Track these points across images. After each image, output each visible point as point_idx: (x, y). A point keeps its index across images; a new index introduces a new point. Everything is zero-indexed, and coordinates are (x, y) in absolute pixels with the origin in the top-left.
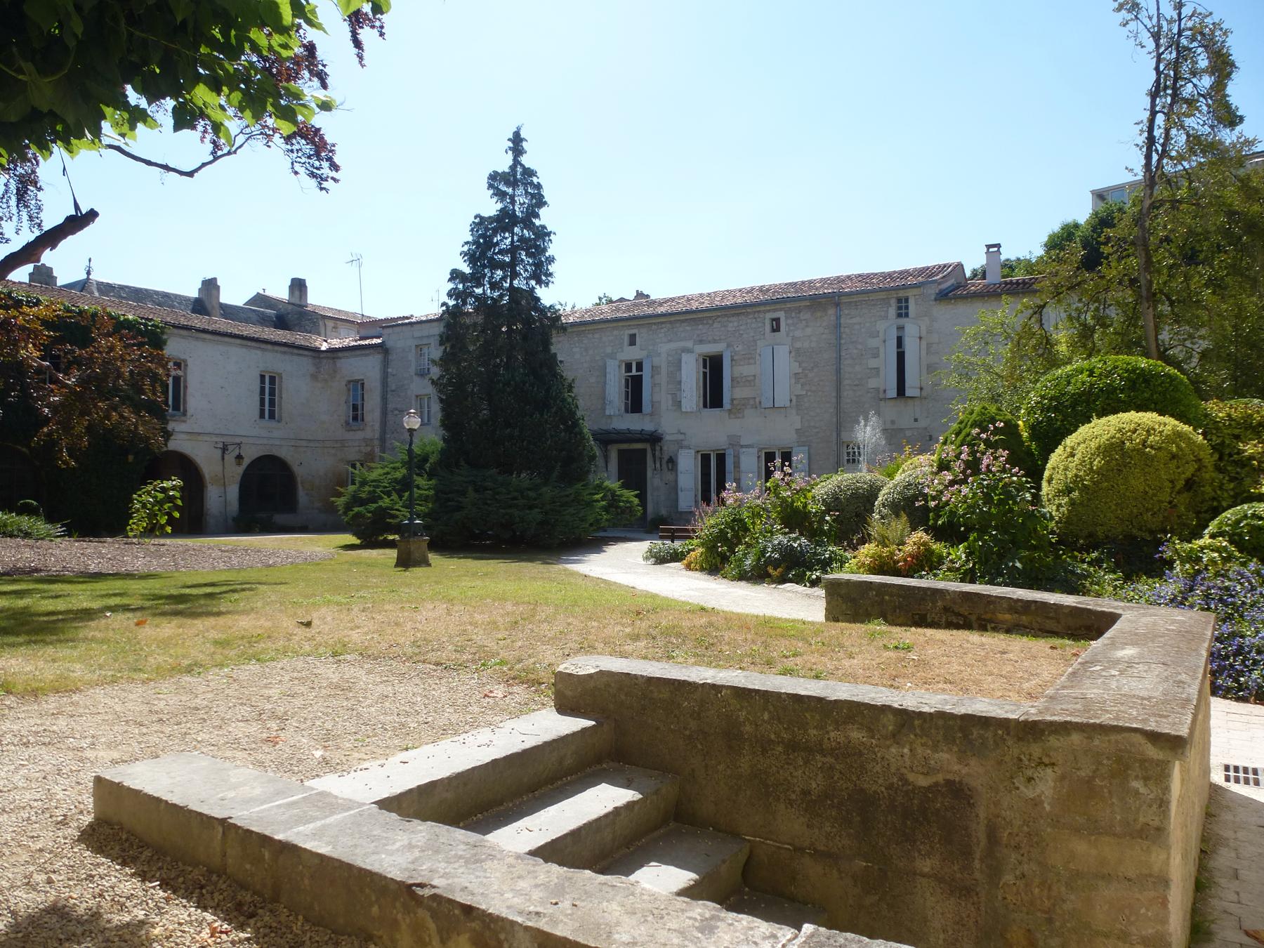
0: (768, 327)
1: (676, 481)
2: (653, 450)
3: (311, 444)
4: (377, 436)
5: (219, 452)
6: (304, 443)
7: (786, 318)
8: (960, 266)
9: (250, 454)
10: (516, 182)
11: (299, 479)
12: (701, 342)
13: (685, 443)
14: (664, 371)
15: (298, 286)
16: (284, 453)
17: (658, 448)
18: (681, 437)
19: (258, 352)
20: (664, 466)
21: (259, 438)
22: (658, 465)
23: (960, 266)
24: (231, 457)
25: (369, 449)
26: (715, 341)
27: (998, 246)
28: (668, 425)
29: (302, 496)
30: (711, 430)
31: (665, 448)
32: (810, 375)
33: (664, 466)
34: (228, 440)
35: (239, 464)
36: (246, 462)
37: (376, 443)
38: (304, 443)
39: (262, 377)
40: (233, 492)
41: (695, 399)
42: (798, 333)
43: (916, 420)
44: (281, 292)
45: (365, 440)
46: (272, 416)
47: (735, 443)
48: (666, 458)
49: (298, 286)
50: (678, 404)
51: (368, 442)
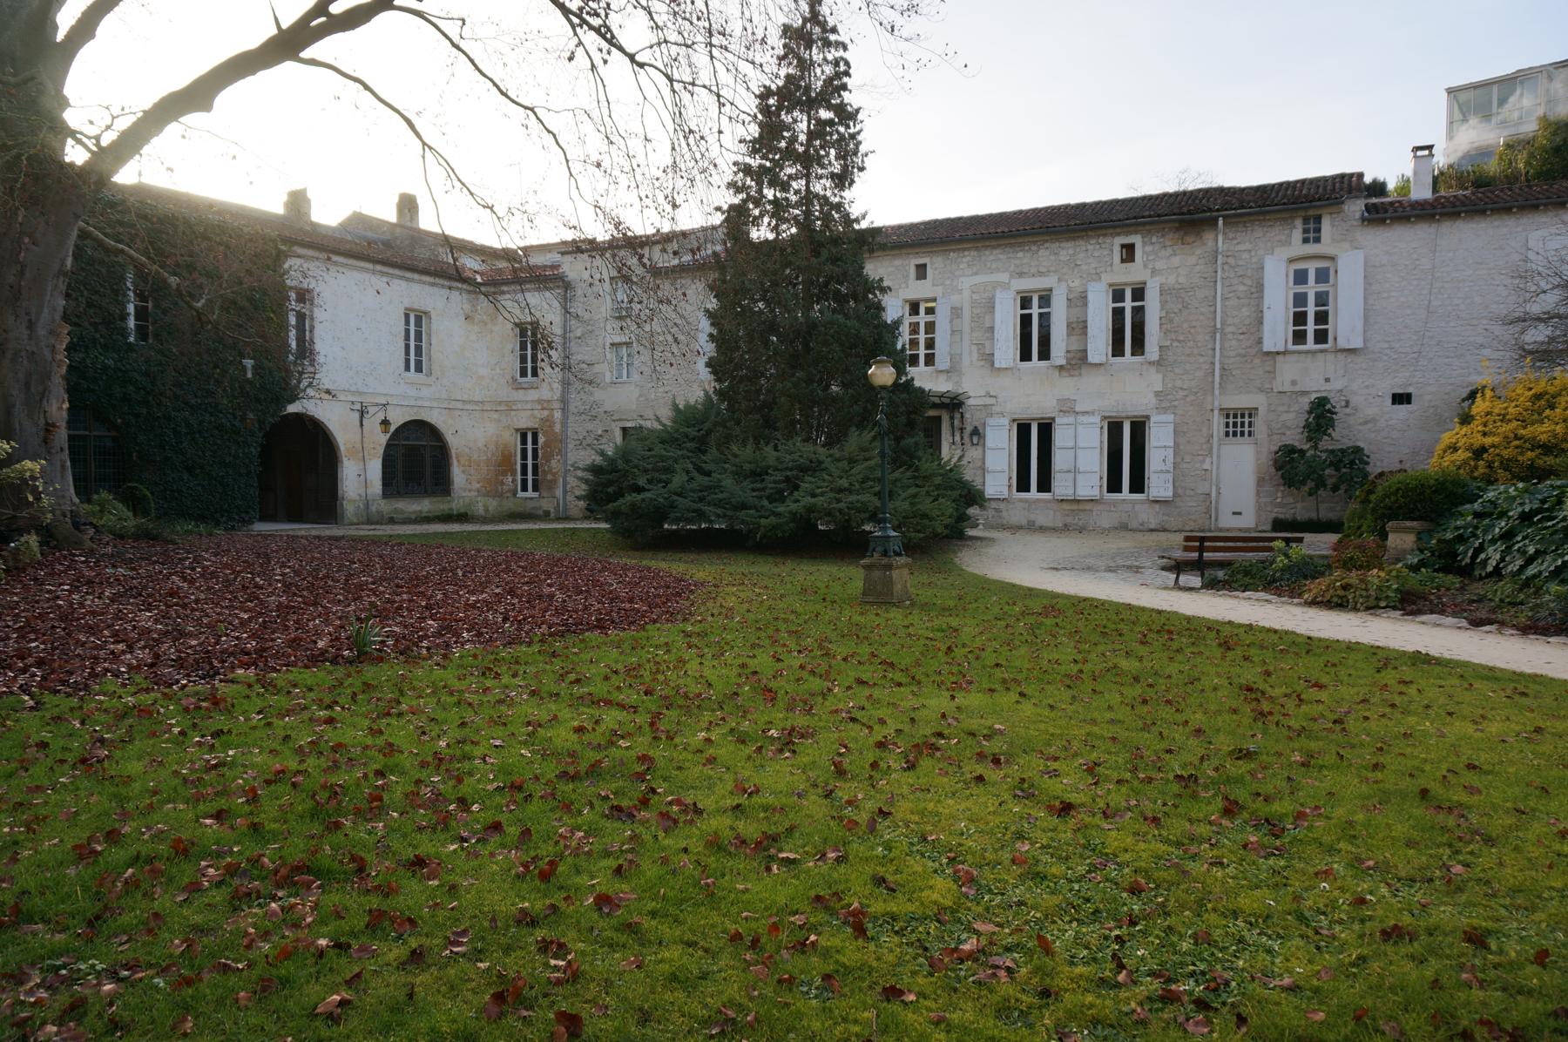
0: (1117, 258)
1: (983, 460)
2: (952, 418)
3: (468, 407)
4: (558, 395)
5: (357, 415)
6: (459, 405)
7: (1144, 244)
8: (1361, 175)
9: (398, 418)
10: (808, 34)
11: (453, 452)
12: (1021, 275)
13: (996, 409)
14: (967, 314)
15: (408, 205)
16: (435, 418)
17: (957, 416)
18: (992, 401)
19: (403, 283)
20: (967, 439)
21: (407, 399)
22: (957, 438)
23: (1361, 175)
24: (372, 423)
25: (546, 413)
26: (1041, 274)
27: (1430, 148)
28: (973, 385)
29: (458, 476)
30: (1030, 391)
31: (967, 416)
32: (1176, 320)
33: (967, 439)
34: (367, 400)
35: (386, 432)
36: (393, 429)
37: (556, 405)
38: (459, 405)
39: (407, 317)
40: (375, 468)
41: (1011, 351)
42: (1159, 265)
43: (1327, 380)
44: (387, 213)
45: (539, 401)
46: (419, 369)
47: (1068, 408)
48: (969, 429)
49: (408, 205)
50: (989, 358)
51: (544, 404)
